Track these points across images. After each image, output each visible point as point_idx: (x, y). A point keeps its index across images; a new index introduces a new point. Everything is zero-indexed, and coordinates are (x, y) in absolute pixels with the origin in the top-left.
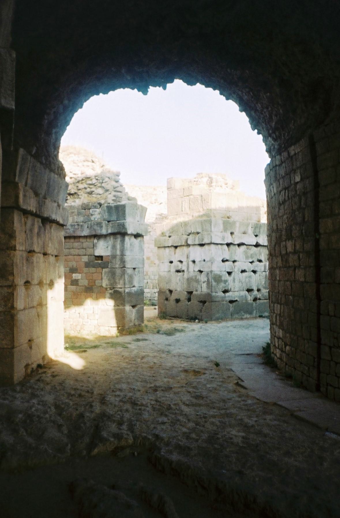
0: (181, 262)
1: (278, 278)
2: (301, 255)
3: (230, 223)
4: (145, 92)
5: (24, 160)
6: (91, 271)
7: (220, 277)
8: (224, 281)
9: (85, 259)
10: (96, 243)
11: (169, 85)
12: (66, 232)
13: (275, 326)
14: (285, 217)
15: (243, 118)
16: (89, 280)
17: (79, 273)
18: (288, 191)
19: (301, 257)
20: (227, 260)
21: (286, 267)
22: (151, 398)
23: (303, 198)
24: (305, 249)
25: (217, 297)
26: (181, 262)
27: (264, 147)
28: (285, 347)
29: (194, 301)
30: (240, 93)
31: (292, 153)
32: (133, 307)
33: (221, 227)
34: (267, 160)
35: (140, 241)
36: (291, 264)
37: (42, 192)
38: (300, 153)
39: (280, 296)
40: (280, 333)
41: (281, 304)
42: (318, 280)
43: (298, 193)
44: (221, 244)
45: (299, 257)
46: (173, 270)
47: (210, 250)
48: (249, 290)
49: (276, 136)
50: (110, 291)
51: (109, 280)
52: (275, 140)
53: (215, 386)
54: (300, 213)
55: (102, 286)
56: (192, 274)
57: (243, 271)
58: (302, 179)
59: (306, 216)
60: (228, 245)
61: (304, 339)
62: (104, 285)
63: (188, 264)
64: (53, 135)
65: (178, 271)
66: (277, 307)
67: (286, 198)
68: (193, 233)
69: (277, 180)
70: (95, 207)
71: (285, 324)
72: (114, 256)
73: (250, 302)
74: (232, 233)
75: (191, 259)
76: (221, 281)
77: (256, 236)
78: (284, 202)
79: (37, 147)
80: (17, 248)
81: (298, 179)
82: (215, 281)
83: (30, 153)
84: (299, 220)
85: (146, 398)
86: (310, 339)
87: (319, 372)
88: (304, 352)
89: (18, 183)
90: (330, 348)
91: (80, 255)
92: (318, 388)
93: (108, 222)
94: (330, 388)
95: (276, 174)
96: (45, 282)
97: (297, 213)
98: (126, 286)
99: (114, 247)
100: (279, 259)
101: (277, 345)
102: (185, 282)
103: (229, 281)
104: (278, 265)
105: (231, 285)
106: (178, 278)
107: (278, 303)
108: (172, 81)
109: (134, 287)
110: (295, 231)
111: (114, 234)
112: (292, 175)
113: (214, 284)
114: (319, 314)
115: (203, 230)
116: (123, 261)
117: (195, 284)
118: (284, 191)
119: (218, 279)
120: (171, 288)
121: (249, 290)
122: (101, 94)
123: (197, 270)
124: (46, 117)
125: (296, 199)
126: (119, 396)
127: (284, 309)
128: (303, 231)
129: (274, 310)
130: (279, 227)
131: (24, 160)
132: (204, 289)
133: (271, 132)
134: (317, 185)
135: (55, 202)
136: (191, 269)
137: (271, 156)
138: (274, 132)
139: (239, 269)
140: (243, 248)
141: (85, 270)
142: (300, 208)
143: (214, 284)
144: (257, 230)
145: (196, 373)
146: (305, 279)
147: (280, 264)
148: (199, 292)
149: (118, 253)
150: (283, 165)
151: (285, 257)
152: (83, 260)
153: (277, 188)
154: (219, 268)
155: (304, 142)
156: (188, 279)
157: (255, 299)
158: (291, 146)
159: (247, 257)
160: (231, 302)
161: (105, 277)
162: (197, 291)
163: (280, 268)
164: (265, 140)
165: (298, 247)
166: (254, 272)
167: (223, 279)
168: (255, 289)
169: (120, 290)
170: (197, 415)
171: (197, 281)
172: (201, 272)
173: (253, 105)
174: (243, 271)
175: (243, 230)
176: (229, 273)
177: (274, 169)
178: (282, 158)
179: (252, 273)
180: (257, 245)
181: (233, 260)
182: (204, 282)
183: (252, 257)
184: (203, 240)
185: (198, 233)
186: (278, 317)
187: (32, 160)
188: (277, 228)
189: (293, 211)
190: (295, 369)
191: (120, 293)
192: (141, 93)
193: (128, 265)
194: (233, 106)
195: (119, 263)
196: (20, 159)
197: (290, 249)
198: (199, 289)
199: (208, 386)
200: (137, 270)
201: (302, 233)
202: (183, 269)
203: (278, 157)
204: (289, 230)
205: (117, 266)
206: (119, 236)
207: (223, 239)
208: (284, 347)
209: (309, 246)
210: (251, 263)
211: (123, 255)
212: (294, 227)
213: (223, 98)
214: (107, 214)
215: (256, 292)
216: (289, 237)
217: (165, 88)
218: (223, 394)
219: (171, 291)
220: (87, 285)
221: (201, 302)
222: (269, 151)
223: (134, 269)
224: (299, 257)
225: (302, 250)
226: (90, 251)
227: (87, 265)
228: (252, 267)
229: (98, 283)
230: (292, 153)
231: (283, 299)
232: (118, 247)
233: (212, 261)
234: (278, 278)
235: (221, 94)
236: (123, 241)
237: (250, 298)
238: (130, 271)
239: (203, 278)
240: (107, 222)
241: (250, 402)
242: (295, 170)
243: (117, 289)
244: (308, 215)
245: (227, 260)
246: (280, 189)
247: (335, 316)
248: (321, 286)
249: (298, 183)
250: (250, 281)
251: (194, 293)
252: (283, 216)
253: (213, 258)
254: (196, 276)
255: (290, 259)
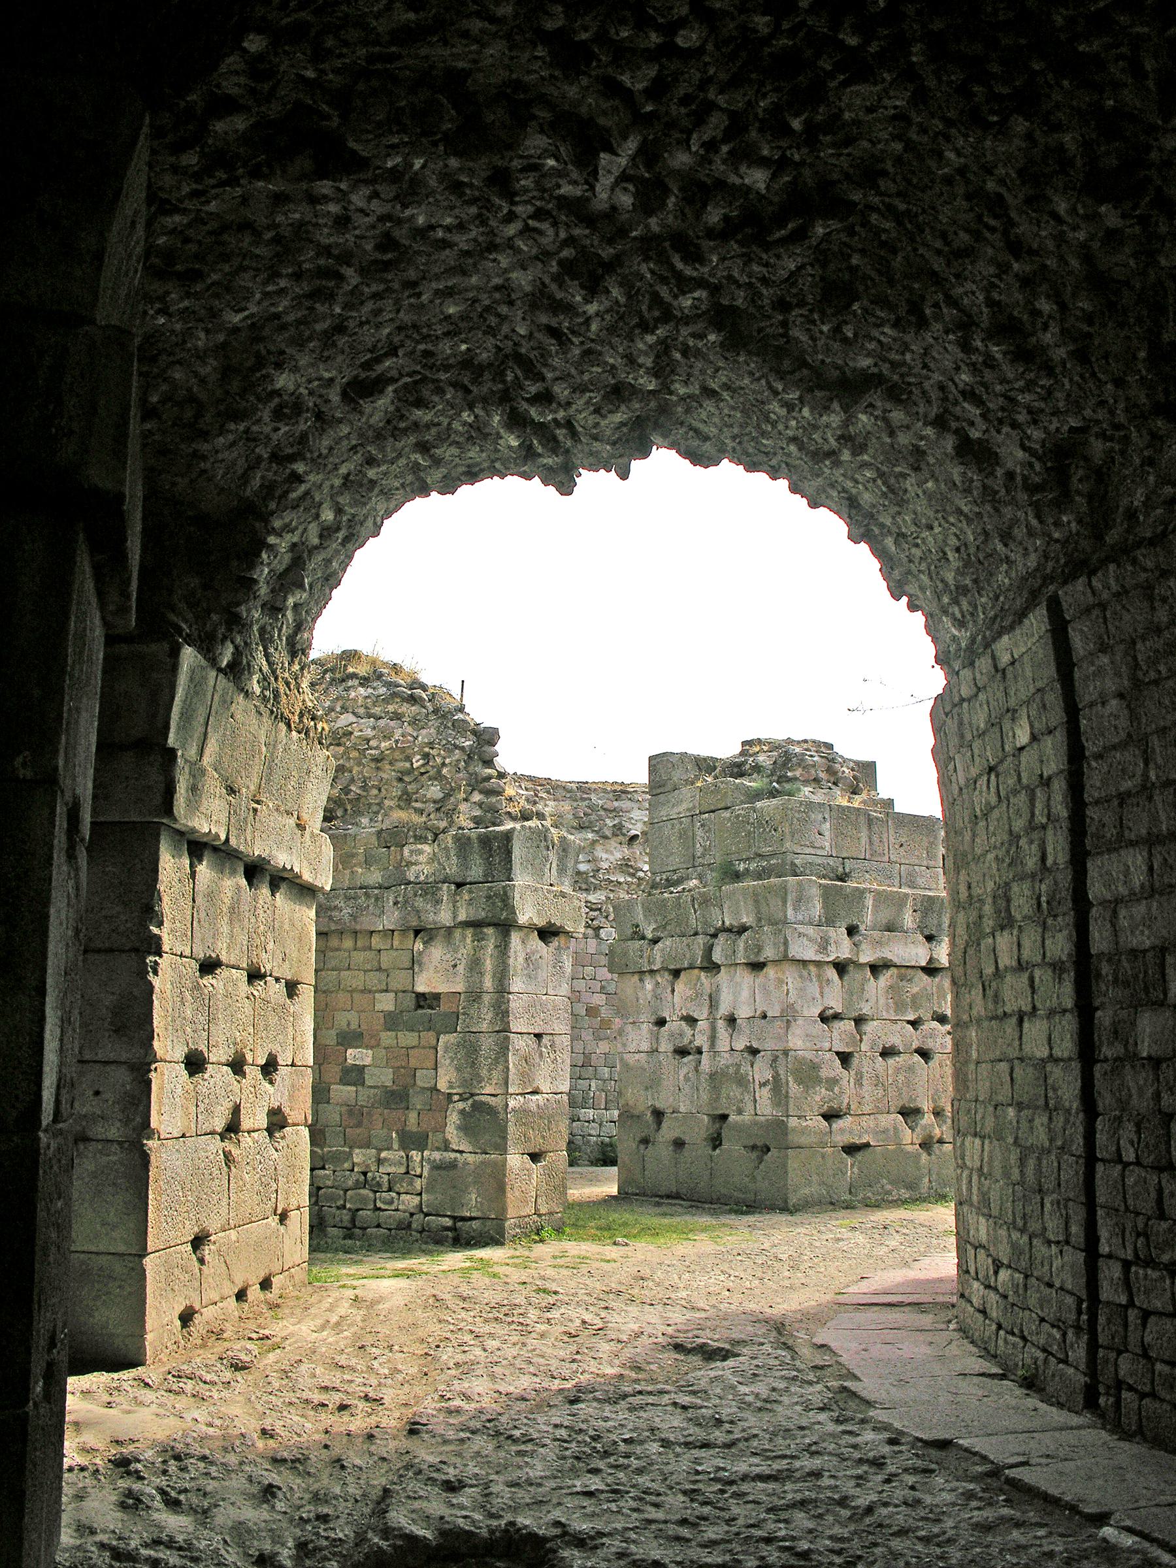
0: (691, 1021)
1: (974, 1055)
2: (1037, 973)
3: (846, 897)
4: (566, 487)
5: (196, 683)
7: (815, 1067)
10: (420, 953)
16: (396, 1069)
17: (367, 1047)
18: (997, 776)
19: (1037, 980)
20: (837, 1017)
21: (995, 1018)
22: (557, 1421)
24: (1048, 954)
25: (804, 1131)
26: (691, 1021)
28: (996, 1273)
29: (732, 1146)
31: (1005, 659)
32: (535, 1157)
33: (817, 909)
35: (558, 948)
36: (1008, 1009)
37: (248, 785)
39: (981, 1111)
40: (982, 1229)
41: (983, 1138)
42: (1087, 1052)
43: (1024, 781)
44: (818, 964)
46: (666, 1047)
47: (780, 982)
48: (909, 1113)
50: (461, 1105)
51: (458, 1069)
54: (1031, 842)
55: (434, 1089)
56: (725, 1059)
57: (887, 1053)
58: (1034, 738)
59: (1050, 849)
60: (841, 968)
61: (1049, 1242)
62: (442, 1085)
63: (713, 1029)
65: (682, 1052)
66: (973, 1145)
70: (420, 839)
73: (909, 1148)
74: (852, 931)
75: (723, 1010)
76: (818, 1081)
77: (930, 938)
80: (166, 948)
82: (799, 1081)
83: (213, 662)
85: (541, 1419)
86: (1067, 1242)
87: (1093, 1347)
88: (1050, 1285)
90: (1126, 1265)
92: (1090, 1402)
93: (459, 885)
94: (1125, 1395)
96: (249, 1059)
97: (1023, 842)
98: (511, 1090)
99: (475, 965)
100: (976, 994)
103: (844, 1082)
104: (974, 1012)
105: (847, 1090)
106: (684, 1071)
107: (975, 1135)
110: (1021, 905)
112: (1007, 725)
113: (794, 1088)
114: (1090, 1159)
115: (760, 920)
116: (502, 1012)
117: (735, 1091)
120: (660, 1105)
123: (740, 1045)
124: (264, 556)
125: (1022, 799)
126: (458, 1411)
127: (990, 1152)
128: (1044, 899)
129: (963, 1159)
133: (946, 600)
134: (1076, 754)
135: (289, 813)
136: (723, 1044)
137: (952, 674)
138: (956, 601)
141: (387, 1038)
142: (1032, 827)
143: (794, 1088)
144: (932, 921)
145: (710, 1354)
146: (1051, 1049)
148: (746, 1117)
149: (488, 983)
151: (994, 984)
155: (1037, 622)
156: (712, 1076)
157: (926, 1145)
158: (1000, 635)
159: (900, 1007)
160: (851, 1149)
163: (979, 1021)
165: (1026, 954)
166: (925, 1054)
167: (824, 1073)
168: (926, 1106)
169: (492, 1101)
170: (698, 1473)
171: (742, 1081)
172: (754, 1052)
174: (887, 1053)
175: (885, 916)
176: (845, 1058)
177: (995, 733)
178: (978, 676)
180: (931, 970)
181: (855, 1014)
182: (763, 1085)
184: (760, 949)
185: (743, 929)
186: (975, 1178)
187: (222, 681)
188: (970, 896)
189: (1014, 838)
190: (1024, 1338)
191: (491, 1111)
194: (830, 525)
195: (489, 1016)
200: (545, 1040)
201: (1039, 904)
202: (697, 1043)
203: (966, 673)
206: (490, 931)
207: (824, 945)
209: (1060, 945)
210: (914, 1024)
213: (800, 502)
215: (928, 1119)
216: (1006, 922)
217: (624, 475)
218: (787, 1412)
219: (658, 1115)
221: (754, 1147)
223: (538, 1036)
226: (399, 980)
228: (915, 1039)
229: (423, 1079)
230: (1005, 659)
232: (488, 965)
233: (789, 1016)
234: (974, 1055)
236: (503, 949)
237: (909, 1138)
238: (520, 1044)
240: (453, 887)
243: (483, 1098)
244: (1058, 847)
245: (837, 1017)
247: (1138, 1163)
248: (1098, 1069)
249: (1022, 749)
253: (791, 1006)
255: (1007, 994)
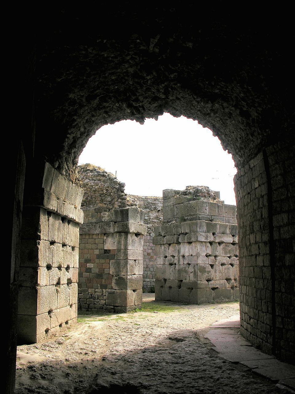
0: (173, 256)
1: (244, 265)
2: (260, 245)
6: (101, 262)
7: (204, 268)
8: (208, 271)
9: (97, 252)
10: (105, 240)
11: (160, 117)
12: (83, 231)
13: (242, 304)
14: (248, 215)
15: (216, 141)
16: (99, 269)
17: (92, 263)
18: (250, 195)
19: (260, 246)
20: (210, 255)
23: (261, 199)
27: (233, 163)
28: (250, 320)
29: (184, 288)
30: (213, 122)
31: (252, 166)
32: (134, 291)
34: (235, 171)
35: (140, 238)
37: (62, 197)
38: (257, 166)
41: (246, 286)
44: (205, 242)
45: (259, 246)
46: (167, 263)
48: (228, 280)
49: (241, 154)
50: (116, 278)
52: (241, 157)
53: (192, 350)
57: (223, 264)
58: (259, 185)
59: (263, 213)
60: (211, 243)
61: (263, 312)
62: (111, 273)
63: (179, 258)
64: (73, 154)
65: (171, 264)
66: (244, 288)
67: (249, 201)
68: (183, 234)
69: (242, 187)
71: (249, 300)
72: (119, 250)
73: (228, 288)
74: (214, 234)
75: (181, 254)
76: (205, 272)
78: (248, 203)
79: (59, 163)
80: (42, 238)
81: (257, 185)
82: (201, 272)
83: (53, 166)
84: (259, 217)
89: (44, 189)
91: (93, 249)
93: (115, 222)
95: (241, 182)
97: (257, 212)
99: (119, 242)
101: (244, 319)
102: (177, 272)
108: (162, 114)
109: (134, 274)
111: (119, 232)
116: (126, 254)
117: (185, 274)
118: (247, 195)
119: (203, 270)
121: (228, 280)
122: (109, 124)
123: (186, 263)
124: (66, 140)
130: (244, 224)
131: (49, 172)
132: (192, 277)
136: (181, 263)
139: (219, 262)
140: (222, 246)
141: (97, 261)
143: (199, 273)
144: (234, 231)
145: (178, 340)
147: (245, 254)
148: (187, 281)
149: (122, 247)
150: (246, 175)
151: (249, 247)
152: (95, 253)
153: (242, 193)
154: (202, 261)
155: (260, 156)
156: (179, 270)
159: (226, 253)
160: (214, 289)
161: (111, 267)
162: (186, 279)
164: (234, 158)
165: (257, 240)
166: (232, 265)
167: (207, 270)
168: (232, 278)
170: (175, 370)
171: (186, 272)
172: (189, 264)
173: (223, 131)
174: (223, 264)
175: (222, 230)
176: (212, 266)
179: (230, 266)
180: (233, 244)
182: (191, 273)
183: (230, 253)
184: (191, 239)
185: (186, 233)
186: (245, 296)
189: (254, 210)
192: (138, 123)
193: (130, 257)
194: (208, 132)
196: (46, 171)
197: (252, 241)
198: (188, 278)
199: (186, 349)
200: (137, 261)
201: (261, 227)
203: (242, 169)
204: (252, 225)
205: (122, 258)
206: (123, 234)
208: (249, 320)
209: (266, 238)
210: (229, 257)
211: (126, 249)
212: (255, 223)
213: (201, 126)
214: (114, 216)
216: (252, 232)
217: (157, 119)
219: (165, 280)
220: (98, 272)
221: (189, 288)
222: (236, 166)
223: (135, 260)
224: (259, 246)
225: (261, 241)
226: (100, 246)
227: (98, 257)
229: (106, 271)
230: (252, 166)
231: (248, 282)
232: (123, 242)
233: (198, 255)
234: (244, 265)
235: (199, 123)
236: (126, 238)
237: (228, 286)
238: (131, 262)
239: (191, 269)
241: (218, 361)
242: (255, 179)
243: (121, 276)
245: (210, 255)
246: (244, 194)
249: (256, 188)
250: (228, 272)
251: (184, 281)
252: (247, 215)
254: (185, 268)
